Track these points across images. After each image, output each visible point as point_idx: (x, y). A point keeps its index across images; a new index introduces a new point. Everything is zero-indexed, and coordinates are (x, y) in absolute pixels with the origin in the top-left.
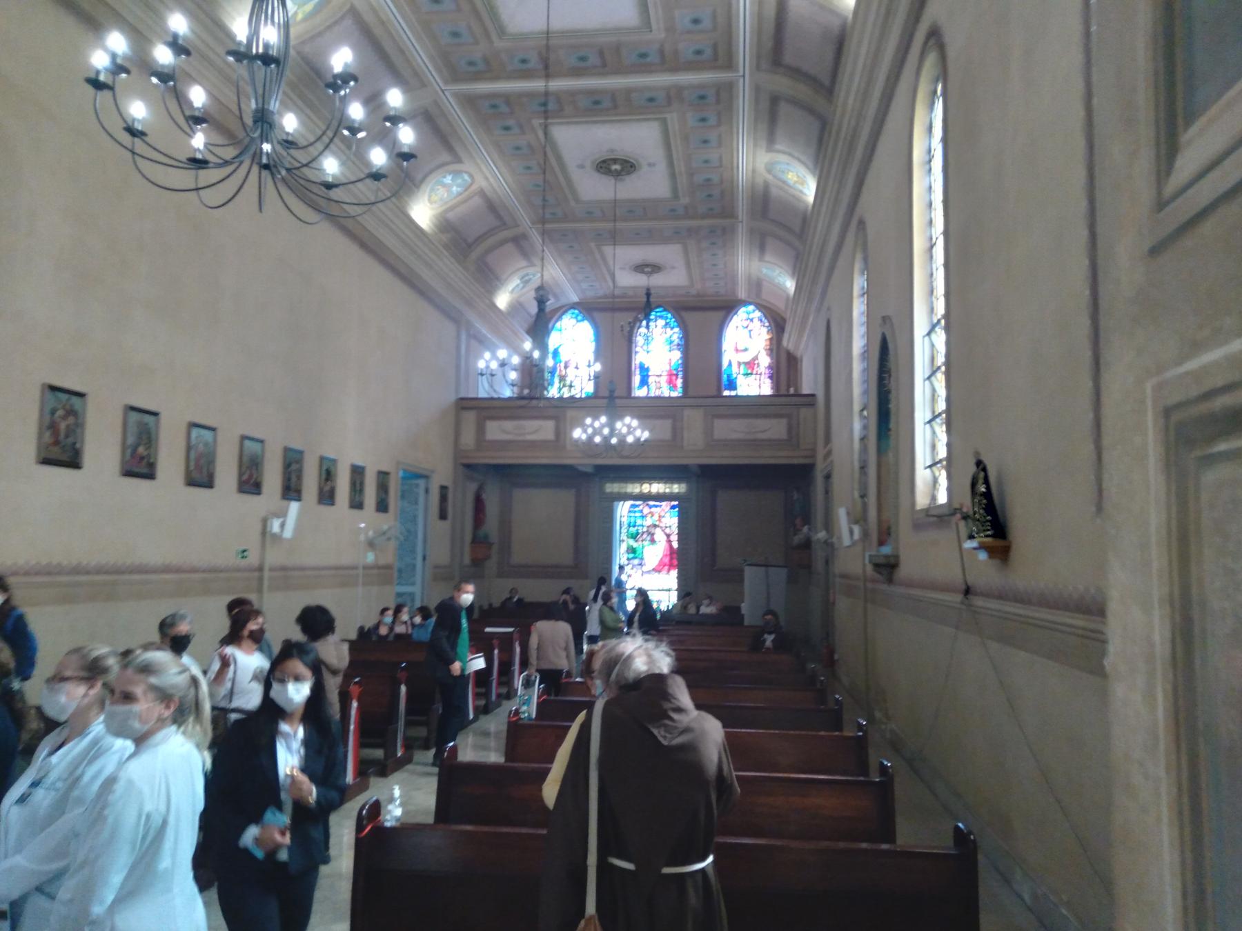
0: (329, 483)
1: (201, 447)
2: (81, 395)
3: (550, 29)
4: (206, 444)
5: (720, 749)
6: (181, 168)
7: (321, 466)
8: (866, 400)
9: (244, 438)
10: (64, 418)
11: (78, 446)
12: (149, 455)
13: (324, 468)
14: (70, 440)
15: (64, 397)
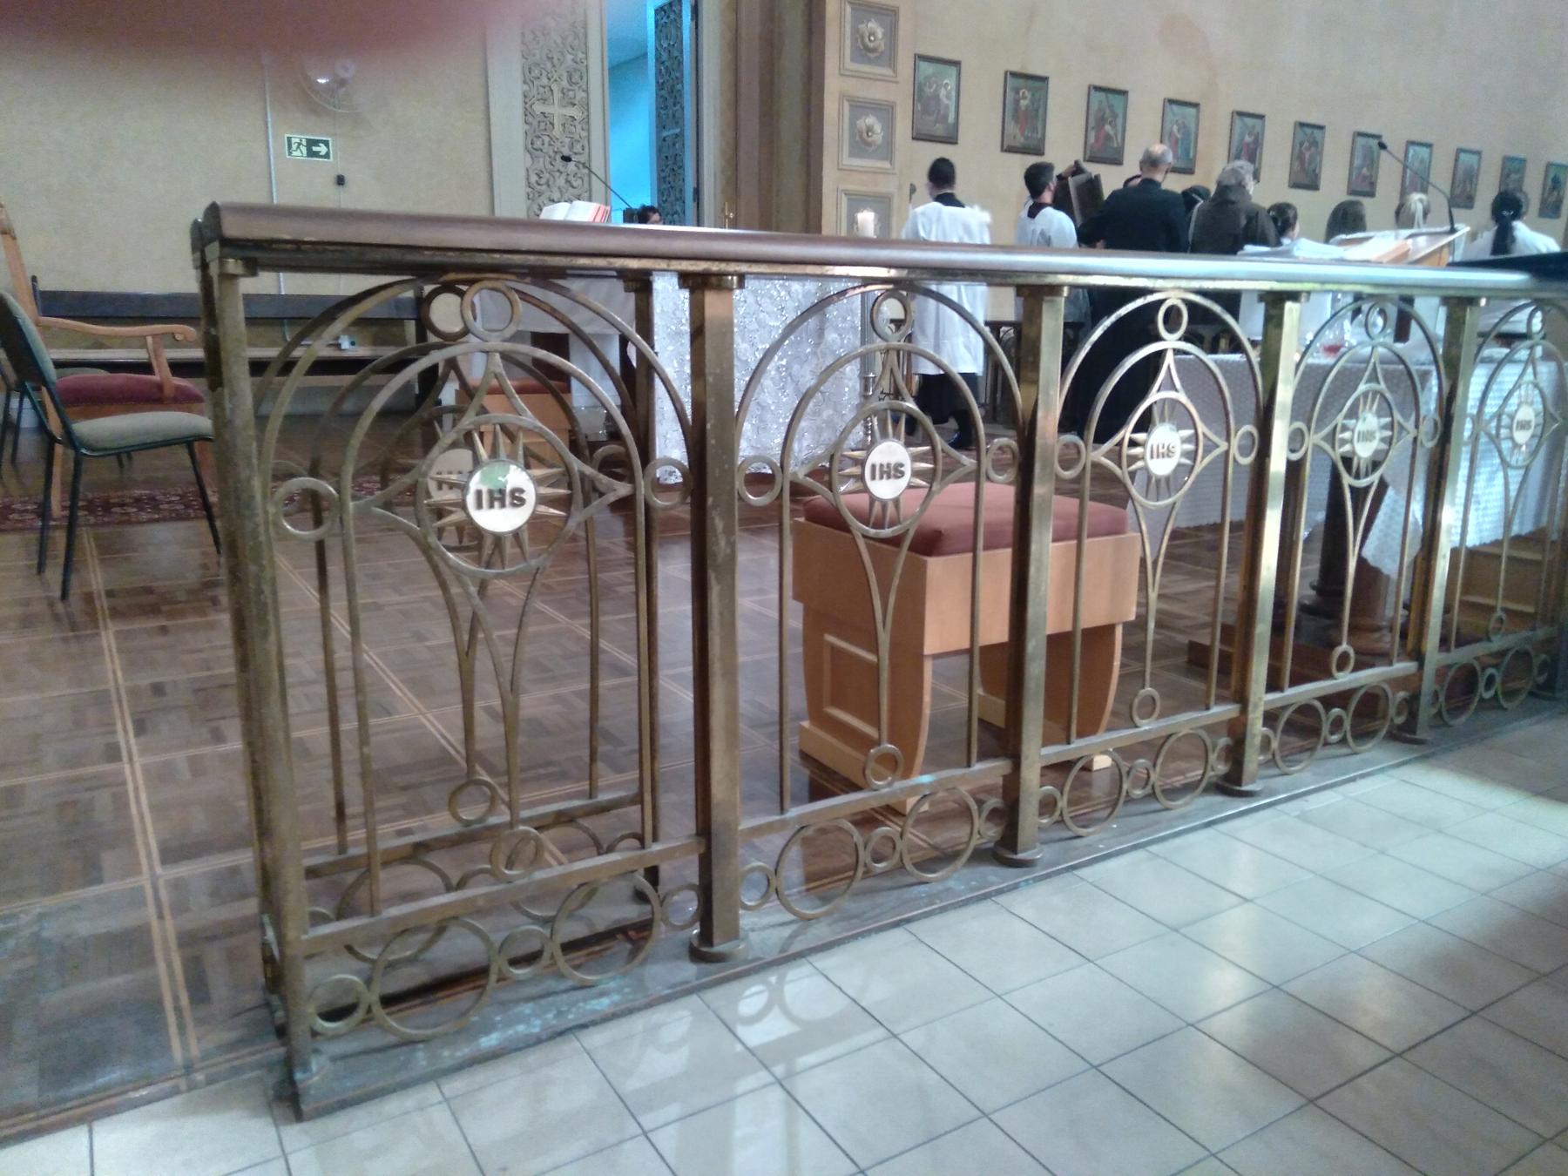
0: (1556, 193)
1: (1416, 164)
2: (1321, 128)
3: (779, 1077)
4: (1422, 161)
5: (1423, 389)
6: (602, 61)
7: (1547, 171)
8: (267, 849)
9: (1460, 151)
10: (1308, 149)
11: (1373, 179)
12: (1371, 176)
13: (1551, 175)
14: (1312, 167)
15: (1309, 131)
